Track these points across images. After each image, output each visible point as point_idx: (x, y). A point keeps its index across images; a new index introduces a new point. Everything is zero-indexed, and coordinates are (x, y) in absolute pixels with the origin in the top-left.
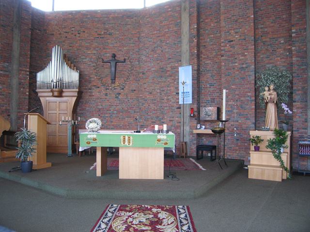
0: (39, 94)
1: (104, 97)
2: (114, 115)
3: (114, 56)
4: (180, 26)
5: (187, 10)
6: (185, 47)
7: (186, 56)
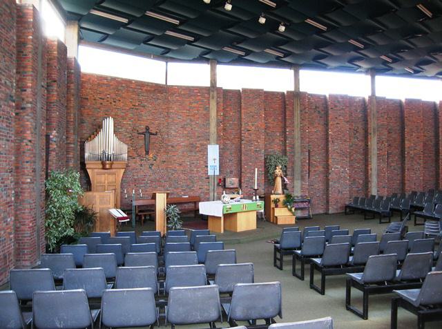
0: (87, 166)
1: (139, 167)
2: (148, 185)
3: (147, 128)
4: (209, 111)
5: (215, 99)
6: (213, 128)
7: (213, 136)
